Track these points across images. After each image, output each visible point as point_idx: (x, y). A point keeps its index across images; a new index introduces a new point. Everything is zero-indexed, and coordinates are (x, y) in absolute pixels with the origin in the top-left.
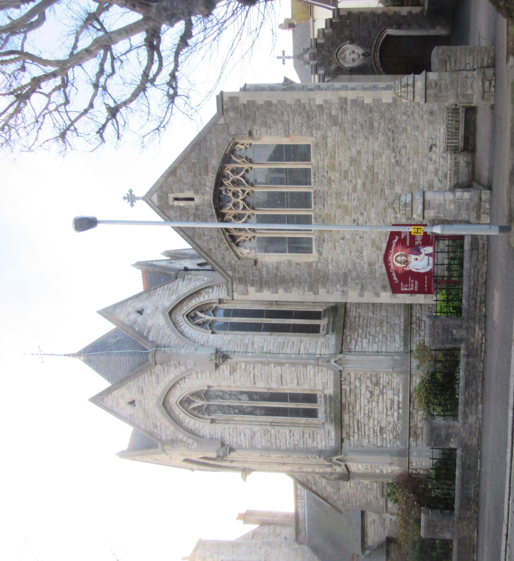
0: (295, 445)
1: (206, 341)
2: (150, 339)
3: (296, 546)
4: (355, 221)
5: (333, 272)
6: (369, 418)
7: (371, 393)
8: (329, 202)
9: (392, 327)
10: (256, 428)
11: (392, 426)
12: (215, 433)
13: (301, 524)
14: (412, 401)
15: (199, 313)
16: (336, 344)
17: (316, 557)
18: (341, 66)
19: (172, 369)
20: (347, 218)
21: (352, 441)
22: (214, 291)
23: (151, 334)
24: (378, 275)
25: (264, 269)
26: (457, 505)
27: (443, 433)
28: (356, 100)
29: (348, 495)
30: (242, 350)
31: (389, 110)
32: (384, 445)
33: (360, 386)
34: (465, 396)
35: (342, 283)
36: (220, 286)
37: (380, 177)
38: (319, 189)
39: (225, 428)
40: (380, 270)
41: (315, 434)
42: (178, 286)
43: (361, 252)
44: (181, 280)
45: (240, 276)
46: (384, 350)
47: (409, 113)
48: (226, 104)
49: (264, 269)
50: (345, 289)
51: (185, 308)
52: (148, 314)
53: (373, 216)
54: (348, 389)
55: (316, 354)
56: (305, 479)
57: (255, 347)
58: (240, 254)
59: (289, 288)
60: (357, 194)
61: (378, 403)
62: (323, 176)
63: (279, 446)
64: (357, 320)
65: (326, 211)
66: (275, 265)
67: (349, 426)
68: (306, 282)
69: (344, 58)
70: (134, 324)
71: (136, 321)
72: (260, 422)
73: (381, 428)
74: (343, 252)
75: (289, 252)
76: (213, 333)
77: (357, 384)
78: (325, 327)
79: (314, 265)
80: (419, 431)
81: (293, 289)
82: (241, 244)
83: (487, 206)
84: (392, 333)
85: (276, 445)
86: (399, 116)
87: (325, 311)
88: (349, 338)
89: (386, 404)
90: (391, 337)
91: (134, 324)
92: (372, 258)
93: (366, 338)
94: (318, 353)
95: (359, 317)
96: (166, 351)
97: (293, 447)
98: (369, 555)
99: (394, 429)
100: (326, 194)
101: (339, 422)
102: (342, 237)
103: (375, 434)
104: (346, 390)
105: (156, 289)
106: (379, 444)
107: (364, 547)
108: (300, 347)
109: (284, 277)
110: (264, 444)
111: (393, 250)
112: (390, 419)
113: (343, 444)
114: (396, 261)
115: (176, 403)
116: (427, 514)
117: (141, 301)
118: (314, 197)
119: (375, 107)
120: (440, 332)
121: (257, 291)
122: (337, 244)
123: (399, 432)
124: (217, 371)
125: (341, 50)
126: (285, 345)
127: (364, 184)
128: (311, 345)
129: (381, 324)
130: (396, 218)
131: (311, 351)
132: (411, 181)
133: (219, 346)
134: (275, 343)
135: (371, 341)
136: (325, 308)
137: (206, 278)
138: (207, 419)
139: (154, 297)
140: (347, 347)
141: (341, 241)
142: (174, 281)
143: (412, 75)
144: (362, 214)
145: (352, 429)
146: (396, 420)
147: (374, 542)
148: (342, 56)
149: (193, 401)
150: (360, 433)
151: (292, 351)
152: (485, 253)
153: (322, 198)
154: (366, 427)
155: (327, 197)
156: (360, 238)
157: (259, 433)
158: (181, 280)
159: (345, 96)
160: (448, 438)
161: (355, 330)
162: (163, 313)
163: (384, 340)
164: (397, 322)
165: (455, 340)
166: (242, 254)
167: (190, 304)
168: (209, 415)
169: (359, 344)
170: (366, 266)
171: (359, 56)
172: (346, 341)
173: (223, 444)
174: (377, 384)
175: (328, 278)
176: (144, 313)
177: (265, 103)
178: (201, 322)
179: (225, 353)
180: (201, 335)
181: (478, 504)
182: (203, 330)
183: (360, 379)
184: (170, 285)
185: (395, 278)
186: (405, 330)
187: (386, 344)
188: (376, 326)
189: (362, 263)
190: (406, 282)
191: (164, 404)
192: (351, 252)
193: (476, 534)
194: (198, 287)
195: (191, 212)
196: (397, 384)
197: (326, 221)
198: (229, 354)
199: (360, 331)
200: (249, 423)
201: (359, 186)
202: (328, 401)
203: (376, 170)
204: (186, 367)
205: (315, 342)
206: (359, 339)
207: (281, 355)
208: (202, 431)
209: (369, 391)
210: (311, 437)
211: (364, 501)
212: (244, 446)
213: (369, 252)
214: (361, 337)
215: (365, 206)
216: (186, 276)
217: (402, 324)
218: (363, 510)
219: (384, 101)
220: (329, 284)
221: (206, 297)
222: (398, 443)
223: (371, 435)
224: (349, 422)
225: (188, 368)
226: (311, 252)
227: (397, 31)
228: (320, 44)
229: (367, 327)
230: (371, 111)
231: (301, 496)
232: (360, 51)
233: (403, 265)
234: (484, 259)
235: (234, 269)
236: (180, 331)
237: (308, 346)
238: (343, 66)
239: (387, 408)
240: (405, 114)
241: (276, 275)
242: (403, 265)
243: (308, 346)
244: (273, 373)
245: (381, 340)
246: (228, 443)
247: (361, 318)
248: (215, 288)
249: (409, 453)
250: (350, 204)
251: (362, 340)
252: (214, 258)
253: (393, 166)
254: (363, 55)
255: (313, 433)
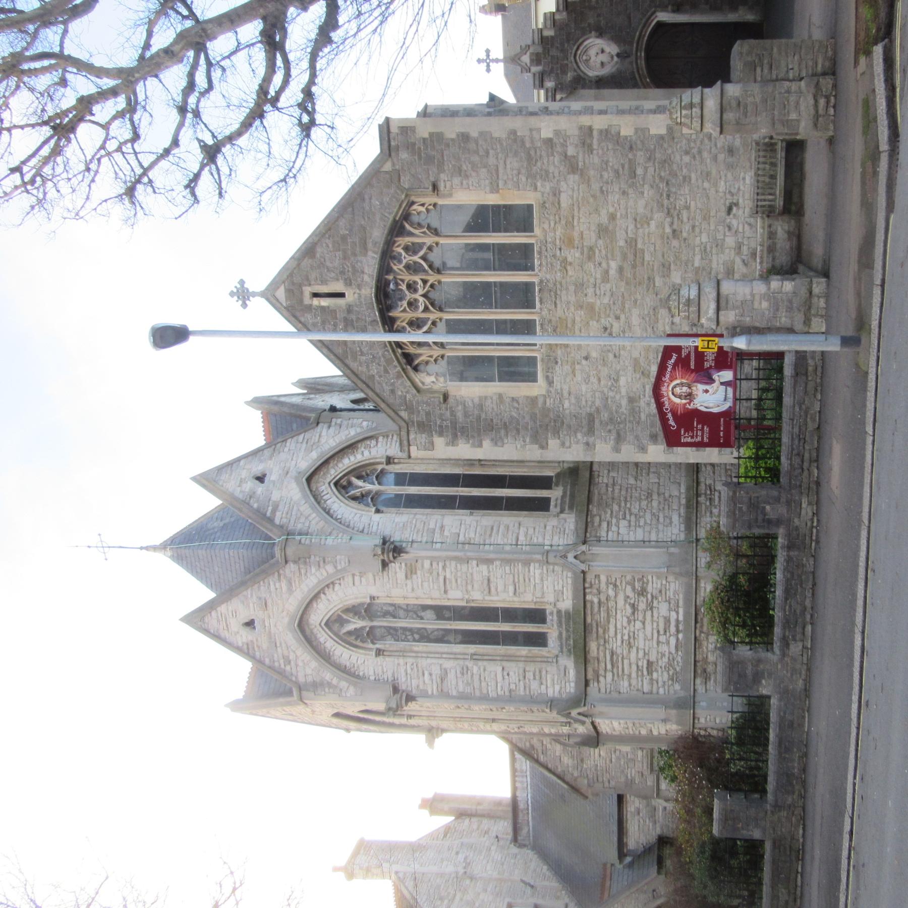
0: (510, 691)
1: (367, 527)
2: (277, 521)
3: (514, 850)
4: (606, 329)
5: (570, 413)
6: (630, 646)
7: (633, 606)
8: (564, 298)
9: (667, 501)
10: (448, 664)
11: (667, 660)
12: (383, 672)
13: (521, 815)
14: (699, 620)
15: (355, 481)
16: (576, 529)
17: (545, 867)
18: (582, 74)
19: (313, 570)
20: (593, 324)
21: (602, 685)
22: (379, 444)
23: (278, 514)
24: (643, 417)
25: (460, 408)
26: (771, 786)
27: (749, 671)
28: (606, 130)
29: (596, 770)
30: (424, 539)
31: (662, 146)
32: (655, 691)
33: (616, 596)
34: (785, 610)
35: (585, 430)
36: (388, 436)
37: (647, 257)
38: (548, 276)
39: (399, 664)
40: (647, 409)
41: (544, 673)
42: (320, 436)
43: (617, 381)
44: (326, 426)
45: (420, 419)
46: (653, 537)
47: (695, 151)
48: (394, 139)
49: (460, 408)
50: (591, 440)
51: (332, 471)
52: (274, 482)
53: (635, 320)
54: (596, 600)
55: (544, 545)
56: (528, 744)
57: (446, 533)
58: (420, 385)
59: (501, 438)
60: (608, 286)
61: (644, 623)
62: (554, 256)
63: (485, 691)
64: (610, 489)
65: (560, 313)
66: (477, 401)
67: (598, 660)
68: (527, 429)
69: (587, 61)
70: (250, 497)
71: (254, 493)
72: (455, 654)
73: (650, 664)
74: (587, 381)
75: (499, 381)
76: (378, 511)
77: (611, 592)
78: (559, 502)
79: (541, 401)
80: (710, 668)
81: (506, 441)
82: (421, 367)
83: (822, 303)
84: (666, 511)
85: (481, 690)
86: (678, 157)
87: (558, 475)
88: (597, 519)
89: (658, 625)
90: (665, 517)
91: (250, 497)
92: (634, 390)
93: (624, 518)
94: (547, 542)
95: (614, 485)
96: (303, 541)
97: (507, 693)
98: (631, 865)
99: (670, 664)
100: (558, 286)
101: (583, 656)
102: (584, 354)
103: (640, 673)
104: (592, 602)
105: (286, 440)
106: (646, 688)
107: (622, 855)
108: (518, 534)
109: (492, 420)
110: (461, 690)
111: (668, 376)
112: (664, 648)
113: (588, 689)
114: (673, 394)
115: (320, 624)
116: (723, 799)
117: (261, 461)
118: (540, 290)
119: (639, 142)
120: (744, 509)
121: (447, 444)
122: (577, 367)
123: (678, 669)
124: (385, 573)
125: (581, 48)
126: (495, 531)
127: (621, 270)
128: (537, 530)
129: (649, 496)
130: (673, 323)
131: (535, 541)
132: (697, 264)
133: (387, 533)
134: (479, 528)
135: (633, 524)
136: (559, 470)
137: (365, 424)
138: (371, 649)
139: (282, 454)
140: (593, 533)
141: (584, 362)
142: (313, 428)
143: (700, 88)
144: (618, 318)
145: (603, 665)
146: (673, 650)
147: (638, 843)
148: (584, 58)
149: (348, 622)
150: (615, 670)
151: (505, 540)
152: (819, 380)
153: (553, 291)
154: (626, 662)
155: (561, 290)
156: (615, 356)
157: (453, 671)
158: (326, 426)
159: (588, 124)
160: (757, 678)
161: (607, 505)
162: (297, 479)
163: (654, 522)
164: (675, 493)
165: (769, 522)
166: (423, 383)
167: (340, 465)
168: (373, 643)
169: (614, 528)
170: (624, 402)
171: (612, 57)
172: (593, 523)
173: (396, 690)
174: (643, 592)
175: (563, 423)
176: (266, 479)
177: (458, 135)
178: (358, 494)
179: (397, 544)
180: (358, 515)
181: (804, 783)
182: (362, 506)
183: (615, 586)
184: (308, 435)
185: (672, 422)
186: (688, 506)
187: (657, 528)
188: (640, 500)
189: (618, 397)
190: (689, 428)
191: (300, 625)
192: (599, 380)
193: (801, 832)
194: (354, 437)
195: (340, 315)
196: (675, 592)
197: (558, 329)
198: (404, 545)
199: (616, 507)
200: (437, 656)
201: (613, 272)
202: (563, 620)
203: (639, 246)
204: (336, 567)
205: (542, 525)
206: (614, 521)
207: (487, 547)
208: (361, 669)
209: (630, 604)
210: (537, 677)
211: (623, 779)
212: (430, 693)
213: (630, 380)
214: (616, 517)
215: (623, 304)
216: (334, 420)
217: (683, 496)
218: (620, 793)
219: (653, 131)
220: (565, 433)
221: (366, 453)
222: (677, 687)
223: (634, 675)
224: (598, 653)
225: (339, 568)
226: (535, 380)
227: (672, 15)
228: (547, 37)
229: (626, 501)
230: (631, 148)
231: (522, 771)
232: (612, 49)
233: (684, 401)
234: (816, 390)
235: (410, 408)
236: (324, 509)
237: (531, 531)
238: (585, 74)
239: (658, 632)
240: (687, 153)
241: (479, 417)
242: (684, 401)
243: (531, 531)
244: (475, 577)
245: (649, 522)
246: (404, 688)
247: (617, 488)
248: (381, 439)
249: (694, 702)
250: (598, 302)
251: (618, 522)
252: (378, 391)
253: (668, 238)
254: (618, 55)
255: (540, 672)
